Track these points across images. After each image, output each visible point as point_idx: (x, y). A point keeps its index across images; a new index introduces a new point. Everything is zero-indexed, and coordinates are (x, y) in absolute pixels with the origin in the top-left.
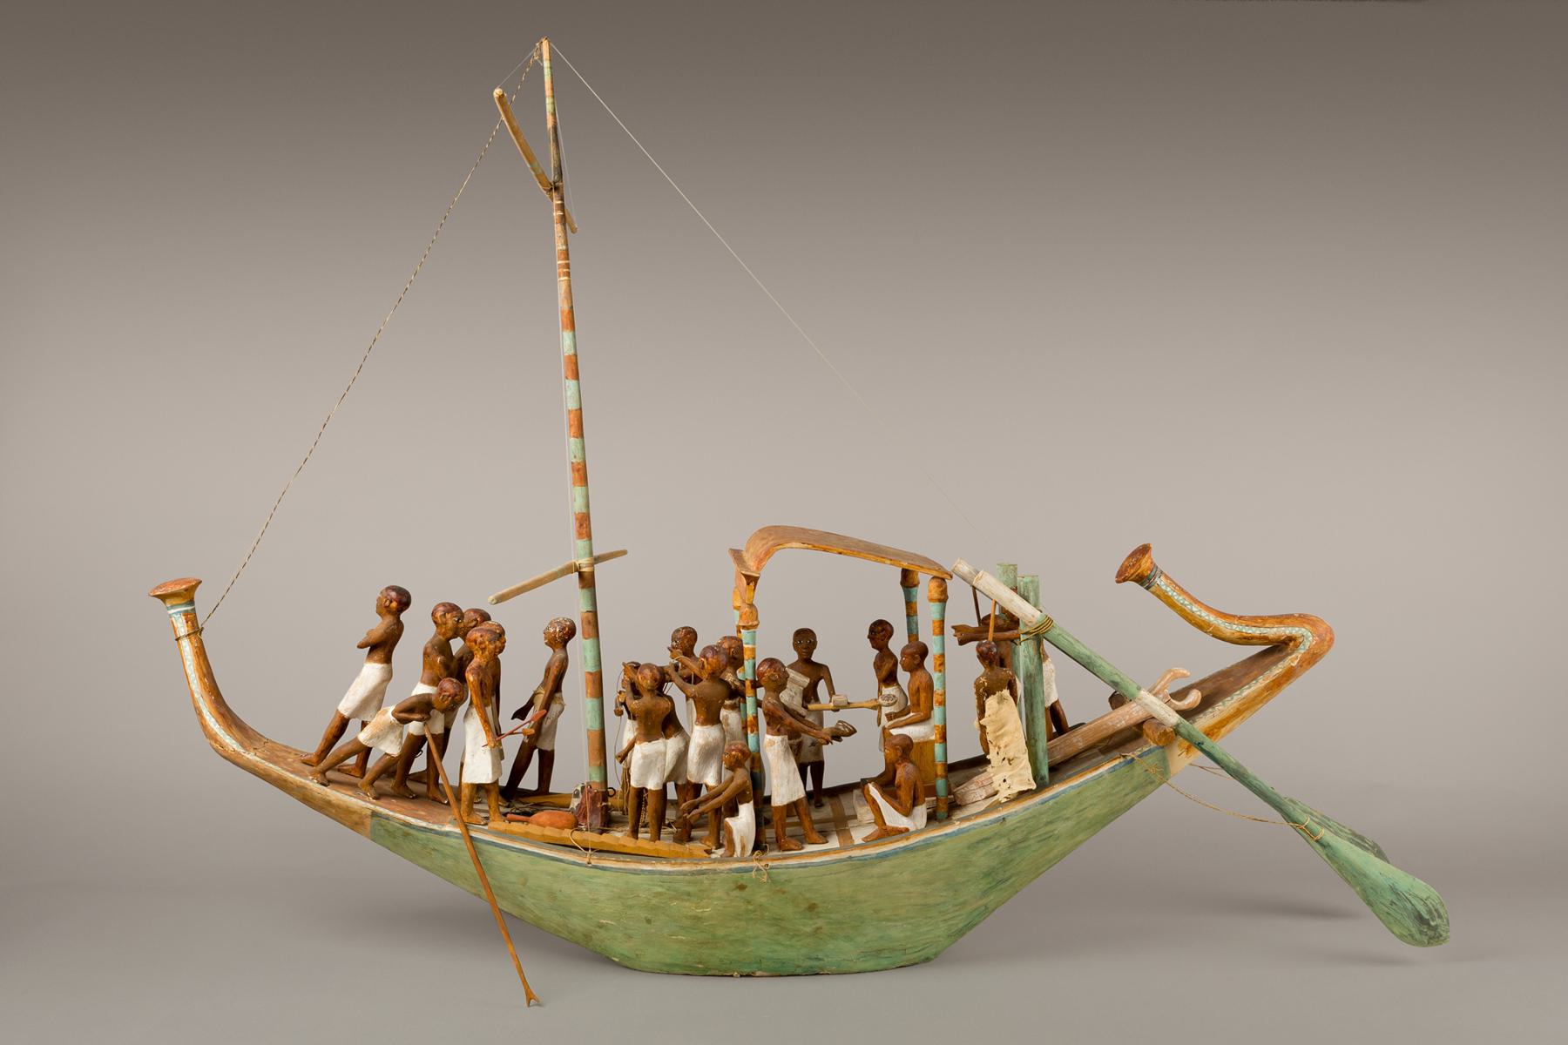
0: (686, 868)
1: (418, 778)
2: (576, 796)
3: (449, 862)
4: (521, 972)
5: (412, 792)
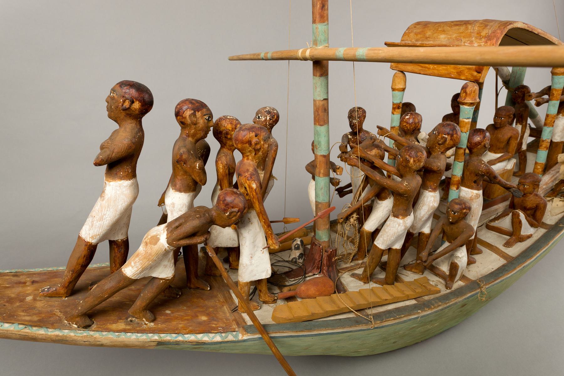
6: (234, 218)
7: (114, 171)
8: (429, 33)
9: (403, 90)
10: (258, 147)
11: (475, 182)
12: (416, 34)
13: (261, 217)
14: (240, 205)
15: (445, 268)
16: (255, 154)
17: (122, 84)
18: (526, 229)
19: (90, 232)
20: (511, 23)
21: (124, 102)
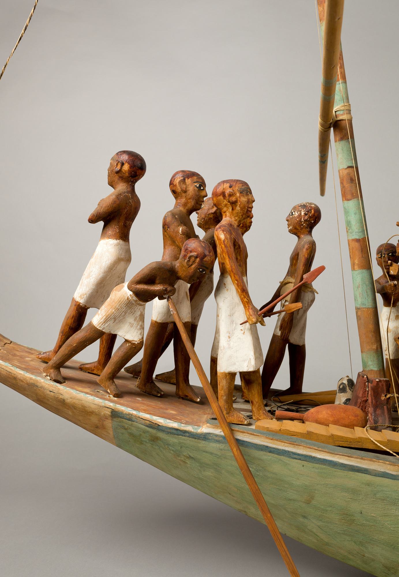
1: (165, 378)
2: (342, 390)
3: (209, 473)
5: (159, 390)
6: (193, 266)
10: (233, 199)
13: (233, 277)
14: (199, 249)
16: (233, 209)
21: (117, 165)
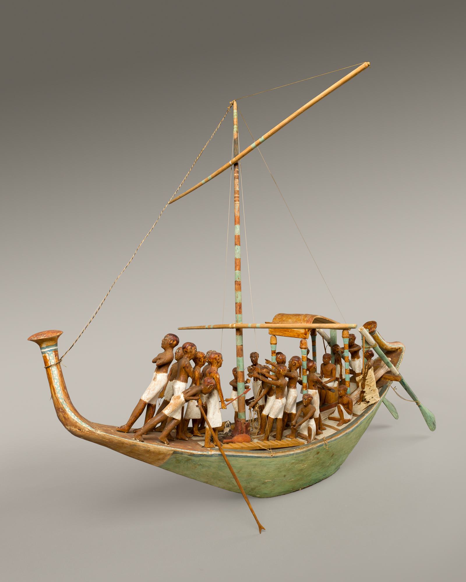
0: (305, 449)
4: (252, 511)
7: (161, 369)
8: (284, 319)
9: (276, 344)
11: (313, 386)
12: (279, 319)
15: (306, 433)
17: (170, 335)
18: (347, 416)
19: (146, 397)
20: (315, 316)
